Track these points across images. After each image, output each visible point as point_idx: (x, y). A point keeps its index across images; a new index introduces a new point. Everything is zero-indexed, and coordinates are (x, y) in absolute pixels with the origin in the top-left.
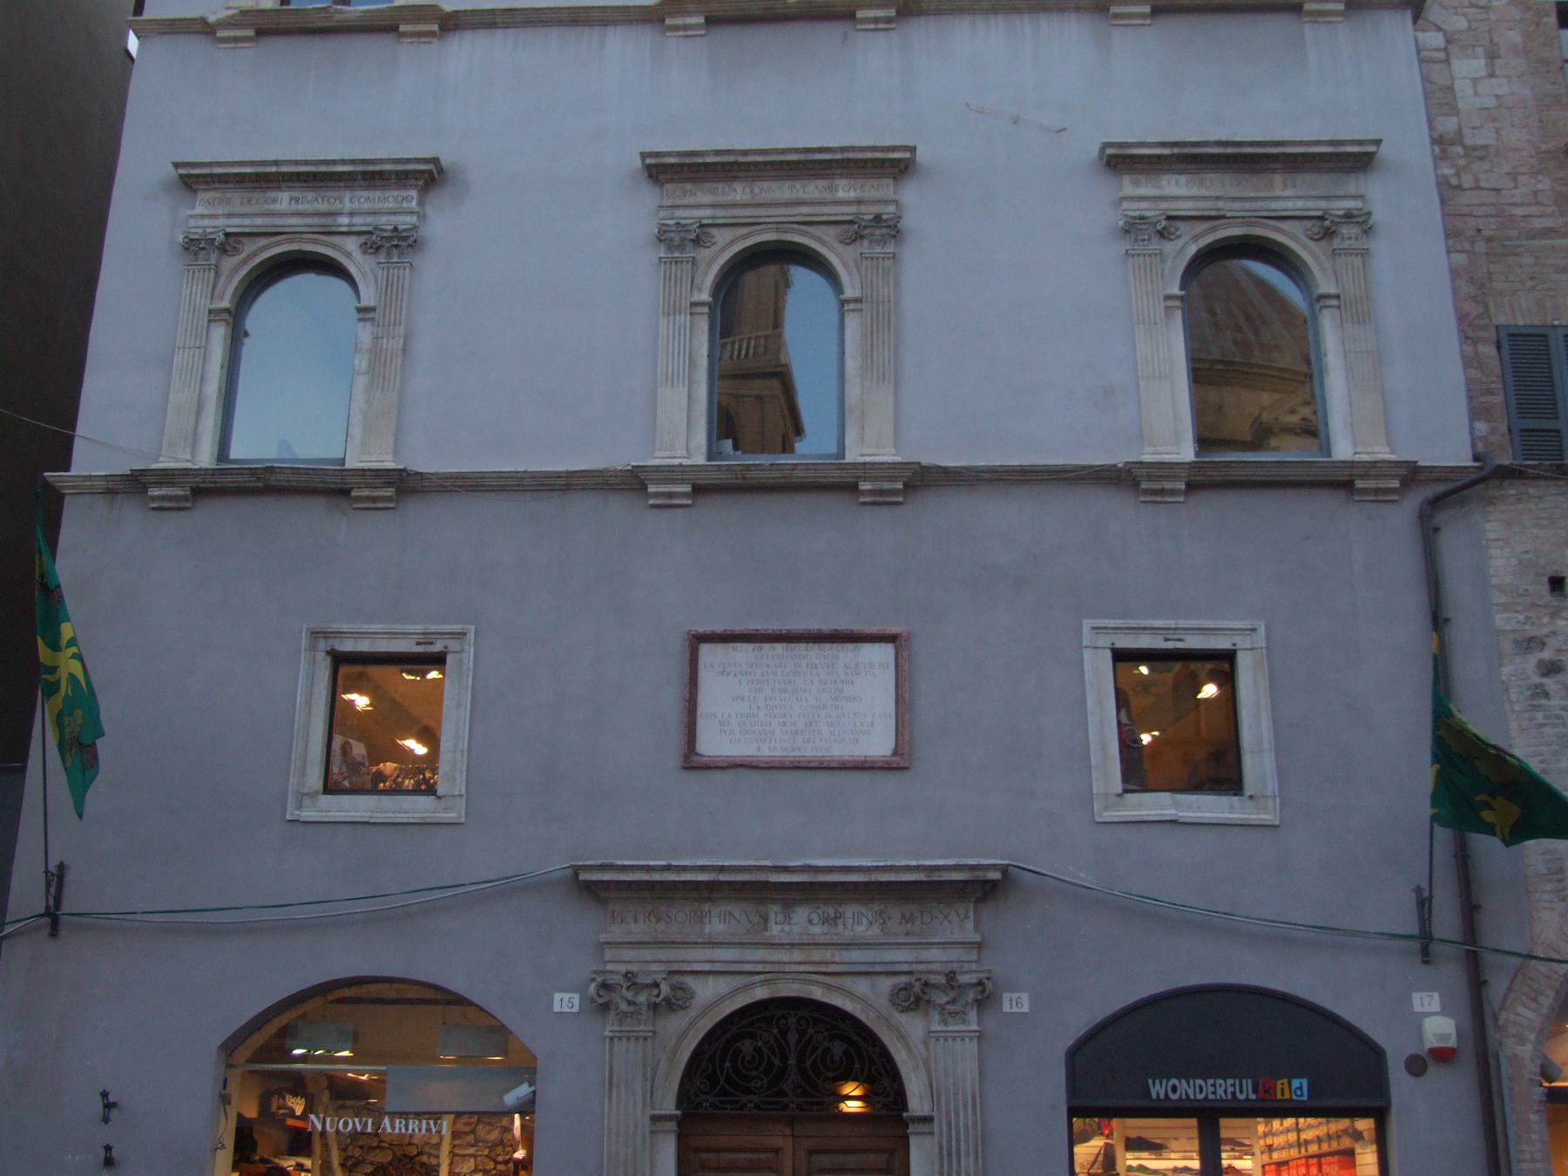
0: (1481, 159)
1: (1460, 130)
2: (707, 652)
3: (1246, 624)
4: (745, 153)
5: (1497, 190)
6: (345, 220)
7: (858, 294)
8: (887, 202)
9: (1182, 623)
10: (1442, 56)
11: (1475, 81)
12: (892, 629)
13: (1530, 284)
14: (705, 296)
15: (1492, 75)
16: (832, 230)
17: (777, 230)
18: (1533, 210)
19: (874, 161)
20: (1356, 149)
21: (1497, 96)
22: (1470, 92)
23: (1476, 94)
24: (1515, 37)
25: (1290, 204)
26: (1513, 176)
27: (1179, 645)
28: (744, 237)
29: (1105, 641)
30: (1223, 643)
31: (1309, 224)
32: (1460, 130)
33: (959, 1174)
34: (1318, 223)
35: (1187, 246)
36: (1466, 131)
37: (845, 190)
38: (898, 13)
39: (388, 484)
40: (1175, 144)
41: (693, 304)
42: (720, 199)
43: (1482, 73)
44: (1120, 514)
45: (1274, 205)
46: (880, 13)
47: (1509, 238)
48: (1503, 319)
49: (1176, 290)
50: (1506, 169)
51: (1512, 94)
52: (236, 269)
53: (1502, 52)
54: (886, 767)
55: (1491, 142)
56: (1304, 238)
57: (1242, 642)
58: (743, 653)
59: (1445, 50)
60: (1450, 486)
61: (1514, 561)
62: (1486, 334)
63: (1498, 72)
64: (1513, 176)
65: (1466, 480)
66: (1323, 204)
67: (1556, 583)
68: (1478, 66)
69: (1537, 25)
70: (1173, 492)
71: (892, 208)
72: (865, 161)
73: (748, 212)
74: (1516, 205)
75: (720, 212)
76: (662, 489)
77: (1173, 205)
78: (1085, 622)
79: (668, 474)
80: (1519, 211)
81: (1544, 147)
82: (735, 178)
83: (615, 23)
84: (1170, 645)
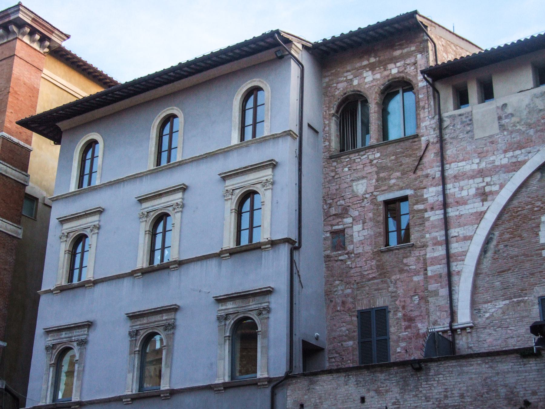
0: (358, 257)
1: (353, 250)
4: (144, 311)
6: (73, 338)
10: (351, 225)
13: (367, 296)
15: (363, 229)
18: (370, 272)
20: (265, 290)
24: (371, 215)
25: (252, 307)
28: (146, 332)
32: (353, 250)
36: (355, 249)
39: (77, 405)
40: (227, 295)
42: (142, 322)
44: (211, 396)
45: (249, 307)
47: (363, 282)
48: (359, 308)
51: (368, 234)
52: (55, 352)
53: (367, 221)
55: (361, 251)
59: (352, 223)
60: (278, 382)
61: (292, 401)
62: (354, 314)
65: (282, 379)
67: (302, 406)
70: (222, 390)
76: (126, 400)
80: (366, 273)
81: (375, 250)
82: (144, 317)
83: (126, 277)
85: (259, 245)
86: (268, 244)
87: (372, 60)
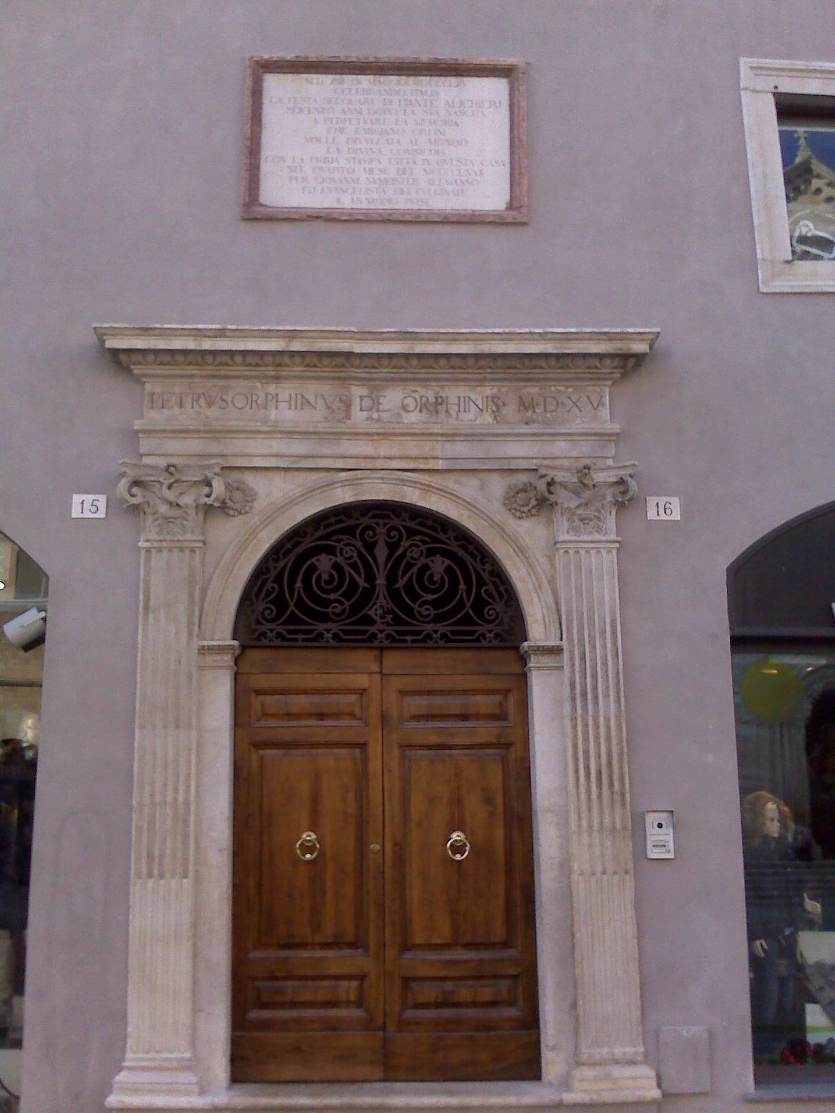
2: (274, 85)
29: (767, 84)
54: (104, 519)
58: (320, 85)
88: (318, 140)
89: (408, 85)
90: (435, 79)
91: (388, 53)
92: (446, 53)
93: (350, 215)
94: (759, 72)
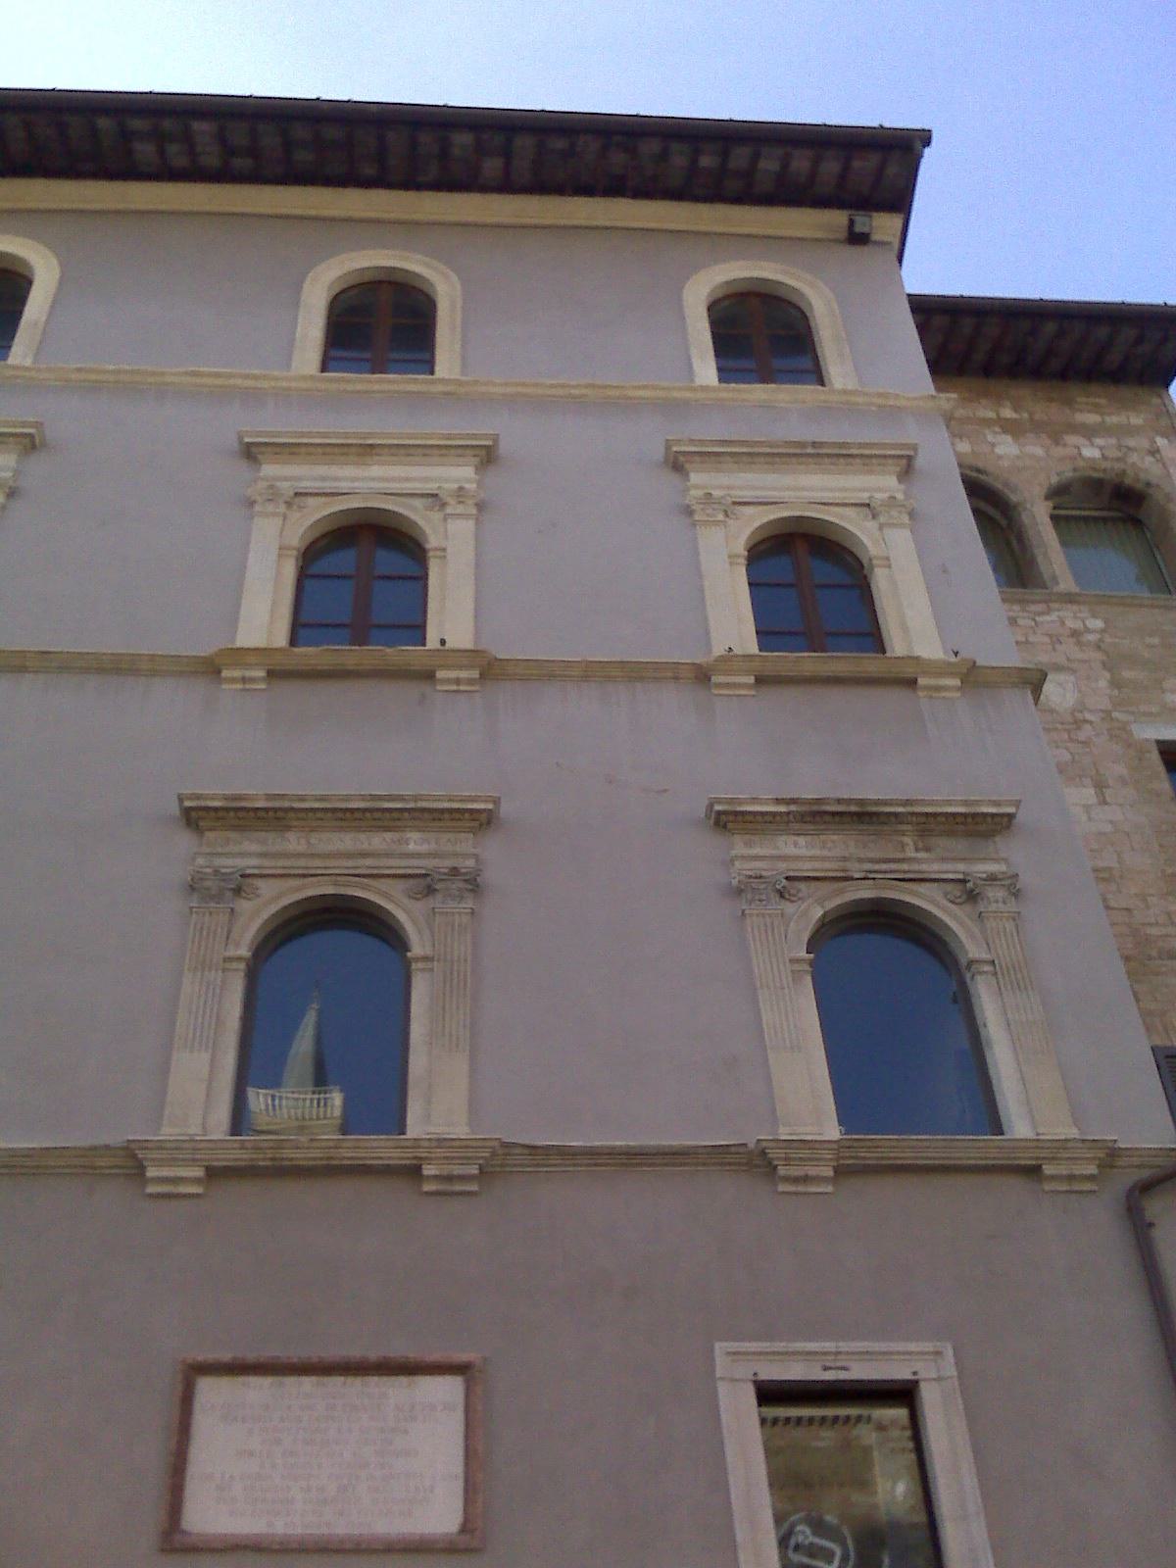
2: (209, 1390)
3: (928, 1346)
5: (1128, 910)
7: (429, 952)
8: (465, 856)
9: (844, 1346)
11: (1087, 808)
12: (462, 1357)
14: (244, 951)
16: (401, 884)
17: (336, 884)
19: (451, 811)
21: (1111, 822)
22: (1084, 818)
23: (1090, 819)
24: (1121, 769)
26: (1143, 897)
27: (842, 1375)
28: (298, 889)
29: (745, 1371)
30: (899, 1372)
31: (949, 887)
33: (1173, 1149)
34: (960, 886)
35: (811, 910)
37: (415, 841)
38: (481, 675)
41: (227, 960)
43: (1093, 800)
46: (463, 674)
49: (803, 954)
50: (1133, 890)
54: (447, 1548)
56: (945, 902)
57: (925, 1371)
58: (258, 1389)
63: (1108, 799)
64: (1143, 897)
66: (961, 867)
68: (1089, 794)
69: (1140, 760)
71: (470, 863)
72: (442, 811)
73: (302, 862)
74: (1150, 924)
75: (266, 863)
76: (165, 1172)
77: (793, 866)
78: (718, 1345)
79: (174, 1151)
82: (288, 828)
84: (829, 1376)
85: (909, 671)
86: (952, 675)
87: (1008, 413)
88: (251, 1454)
89: (355, 1385)
90: (385, 1379)
91: (354, 1352)
92: (400, 1348)
93: (281, 1543)
94: (735, 1357)
